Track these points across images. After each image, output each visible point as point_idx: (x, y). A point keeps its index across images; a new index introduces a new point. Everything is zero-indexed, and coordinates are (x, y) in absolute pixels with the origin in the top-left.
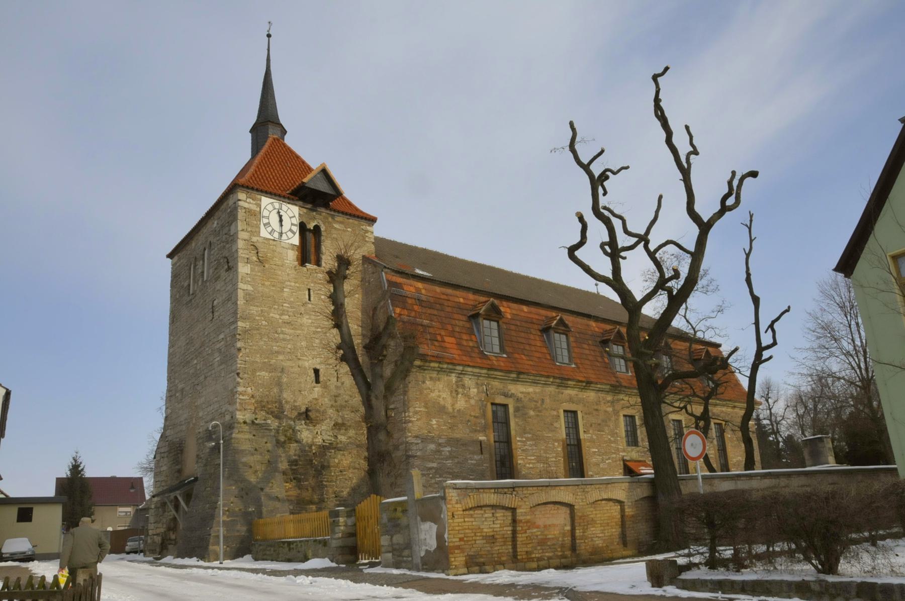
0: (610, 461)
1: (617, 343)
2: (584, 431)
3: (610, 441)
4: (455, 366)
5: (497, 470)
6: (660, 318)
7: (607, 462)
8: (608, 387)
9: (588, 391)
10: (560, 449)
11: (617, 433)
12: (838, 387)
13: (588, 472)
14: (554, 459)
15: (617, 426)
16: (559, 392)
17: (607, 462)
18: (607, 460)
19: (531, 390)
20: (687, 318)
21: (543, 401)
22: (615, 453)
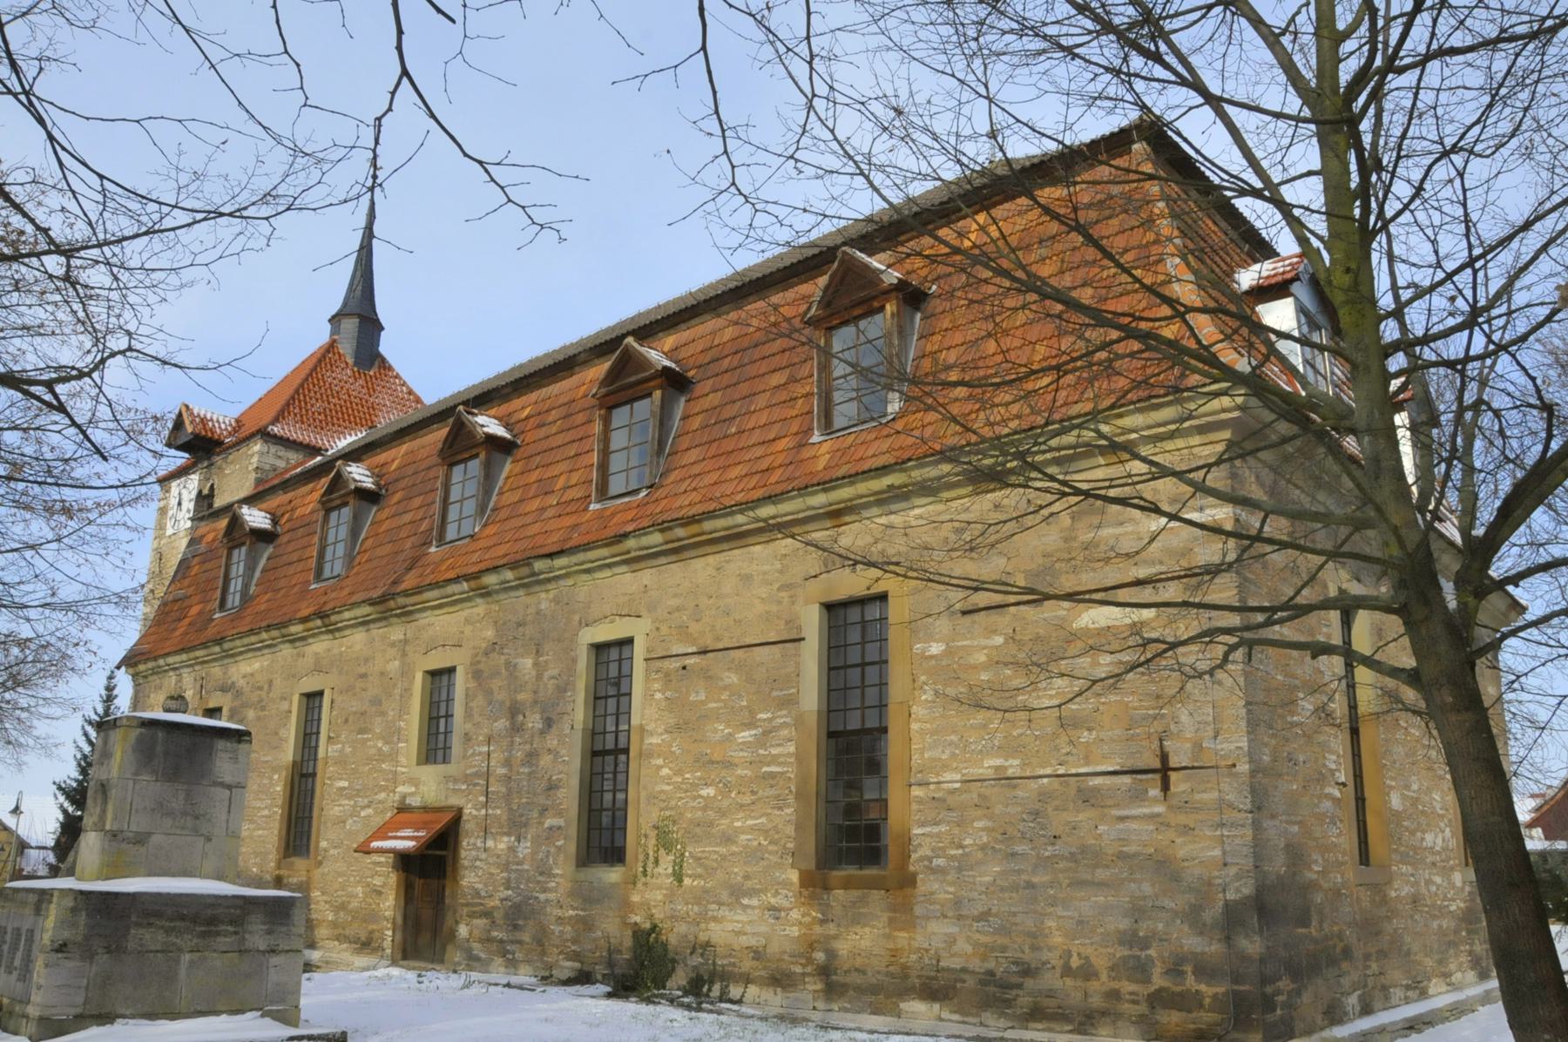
0: (370, 811)
1: (459, 457)
2: (329, 738)
3: (382, 757)
4: (479, 578)
5: (930, 480)
6: (1486, 533)
7: (363, 814)
8: (367, 609)
9: (417, 616)
10: (278, 789)
11: (399, 730)
12: (226, 756)
13: (318, 842)
14: (266, 812)
15: (403, 710)
16: (298, 655)
17: (363, 814)
18: (363, 808)
19: (257, 665)
20: (809, 227)
21: (270, 683)
22: (384, 789)
